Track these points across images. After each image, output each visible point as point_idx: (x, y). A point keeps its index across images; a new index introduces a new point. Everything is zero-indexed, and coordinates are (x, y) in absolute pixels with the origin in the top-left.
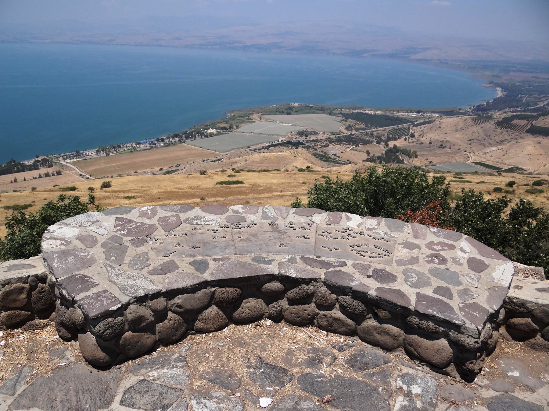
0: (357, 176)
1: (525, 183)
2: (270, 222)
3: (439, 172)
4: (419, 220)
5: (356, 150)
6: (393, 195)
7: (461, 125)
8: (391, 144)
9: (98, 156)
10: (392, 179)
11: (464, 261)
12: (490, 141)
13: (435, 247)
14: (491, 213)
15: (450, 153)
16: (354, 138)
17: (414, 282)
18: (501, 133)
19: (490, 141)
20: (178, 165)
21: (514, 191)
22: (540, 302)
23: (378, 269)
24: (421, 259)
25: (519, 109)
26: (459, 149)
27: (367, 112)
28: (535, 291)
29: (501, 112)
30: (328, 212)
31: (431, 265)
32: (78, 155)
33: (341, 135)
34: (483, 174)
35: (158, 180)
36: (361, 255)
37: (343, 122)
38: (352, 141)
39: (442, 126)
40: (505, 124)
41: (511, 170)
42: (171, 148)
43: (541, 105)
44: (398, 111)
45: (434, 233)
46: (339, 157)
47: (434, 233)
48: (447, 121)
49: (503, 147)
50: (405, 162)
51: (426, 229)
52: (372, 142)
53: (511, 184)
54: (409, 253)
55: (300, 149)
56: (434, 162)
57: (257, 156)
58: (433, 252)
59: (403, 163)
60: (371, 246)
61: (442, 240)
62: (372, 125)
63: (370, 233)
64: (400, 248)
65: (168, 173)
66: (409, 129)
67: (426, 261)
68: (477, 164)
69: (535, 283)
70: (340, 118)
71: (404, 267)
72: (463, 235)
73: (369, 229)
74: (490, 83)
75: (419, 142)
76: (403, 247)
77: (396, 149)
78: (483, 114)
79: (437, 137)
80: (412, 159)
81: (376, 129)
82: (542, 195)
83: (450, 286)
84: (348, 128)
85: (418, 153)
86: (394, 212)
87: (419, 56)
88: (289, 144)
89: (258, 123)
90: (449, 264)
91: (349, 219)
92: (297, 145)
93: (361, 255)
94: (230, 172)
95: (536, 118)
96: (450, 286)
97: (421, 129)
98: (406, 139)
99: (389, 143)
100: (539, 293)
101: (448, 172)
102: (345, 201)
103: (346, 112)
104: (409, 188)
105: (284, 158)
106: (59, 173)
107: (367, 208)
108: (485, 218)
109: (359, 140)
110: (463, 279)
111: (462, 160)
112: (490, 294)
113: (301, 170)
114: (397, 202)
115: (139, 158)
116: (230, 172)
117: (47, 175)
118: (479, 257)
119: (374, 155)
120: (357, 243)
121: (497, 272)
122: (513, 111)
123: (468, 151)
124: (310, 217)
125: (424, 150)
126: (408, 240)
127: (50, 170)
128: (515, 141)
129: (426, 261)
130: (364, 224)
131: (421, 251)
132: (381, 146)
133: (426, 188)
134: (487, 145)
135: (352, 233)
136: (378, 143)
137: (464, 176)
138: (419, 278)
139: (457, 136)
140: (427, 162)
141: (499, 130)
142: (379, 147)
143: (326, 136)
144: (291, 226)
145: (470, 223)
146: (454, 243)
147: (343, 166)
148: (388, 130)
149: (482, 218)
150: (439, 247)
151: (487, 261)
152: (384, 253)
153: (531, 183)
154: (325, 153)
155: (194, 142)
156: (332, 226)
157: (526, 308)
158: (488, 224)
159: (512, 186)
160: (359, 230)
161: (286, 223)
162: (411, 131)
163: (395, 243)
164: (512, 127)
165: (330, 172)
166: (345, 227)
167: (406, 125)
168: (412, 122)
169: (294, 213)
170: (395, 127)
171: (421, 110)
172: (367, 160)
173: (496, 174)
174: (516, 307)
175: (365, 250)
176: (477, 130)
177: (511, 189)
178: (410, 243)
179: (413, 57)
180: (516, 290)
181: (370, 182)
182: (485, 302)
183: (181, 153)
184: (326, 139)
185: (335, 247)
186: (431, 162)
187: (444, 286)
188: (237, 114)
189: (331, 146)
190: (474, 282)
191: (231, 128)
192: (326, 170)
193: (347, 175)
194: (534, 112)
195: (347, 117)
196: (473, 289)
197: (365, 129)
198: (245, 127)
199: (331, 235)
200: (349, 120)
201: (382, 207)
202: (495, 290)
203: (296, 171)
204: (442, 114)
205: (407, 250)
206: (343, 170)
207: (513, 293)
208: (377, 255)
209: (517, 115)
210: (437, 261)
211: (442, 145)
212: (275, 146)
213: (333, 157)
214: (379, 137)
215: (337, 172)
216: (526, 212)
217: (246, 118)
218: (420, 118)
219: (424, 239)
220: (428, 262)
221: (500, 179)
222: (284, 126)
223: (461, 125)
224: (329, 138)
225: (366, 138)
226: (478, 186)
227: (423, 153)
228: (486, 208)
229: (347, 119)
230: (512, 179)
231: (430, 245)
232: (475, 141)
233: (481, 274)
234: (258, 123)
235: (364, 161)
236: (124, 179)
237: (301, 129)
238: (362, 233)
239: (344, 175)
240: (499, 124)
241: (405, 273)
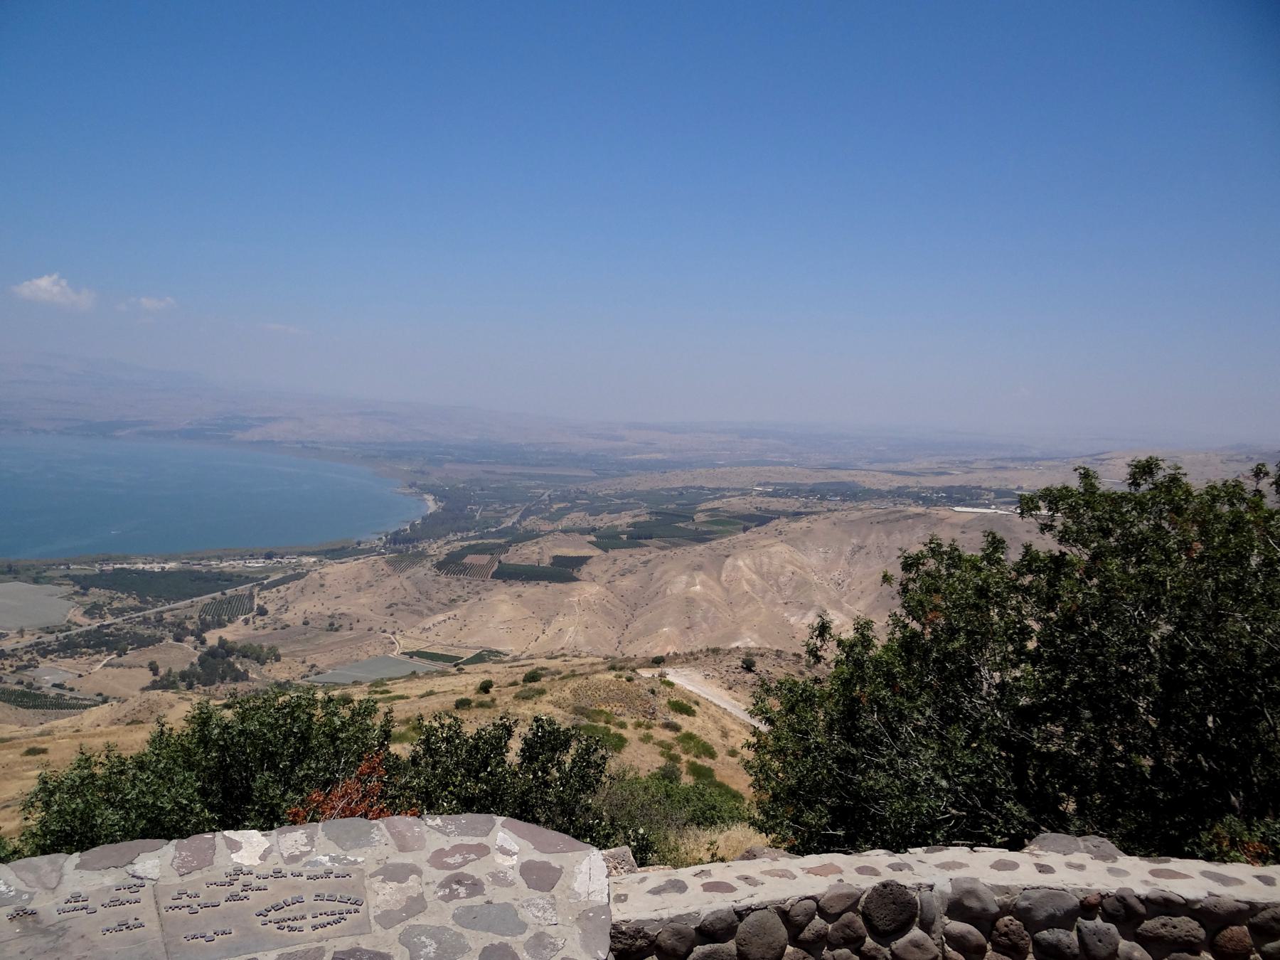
0: (162, 733)
1: (511, 680)
2: (10, 910)
3: (336, 685)
4: (343, 810)
5: (120, 666)
6: (269, 759)
7: (368, 576)
8: (212, 638)
10: (261, 724)
11: (514, 875)
12: (430, 604)
13: (450, 860)
14: (488, 756)
15: (351, 640)
16: (107, 635)
17: (432, 955)
18: (448, 585)
19: (430, 604)
21: (493, 700)
22: (665, 915)
23: (343, 952)
24: (429, 897)
25: (472, 534)
26: (370, 630)
27: (141, 566)
28: (650, 896)
29: (440, 543)
30: (174, 842)
31: (455, 904)
33: (73, 632)
34: (429, 674)
36: (291, 929)
37: (77, 598)
38: (106, 644)
39: (327, 583)
40: (451, 565)
41: (479, 659)
43: (509, 523)
44: (221, 559)
45: (438, 829)
46: (72, 690)
47: (438, 829)
48: (336, 570)
49: (457, 612)
50: (252, 675)
51: (419, 826)
52: (161, 640)
53: (485, 688)
54: (400, 889)
56: (321, 666)
58: (448, 873)
59: (247, 679)
60: (309, 899)
61: (457, 840)
62: (158, 598)
63: (296, 867)
64: (376, 883)
66: (251, 597)
67: (443, 898)
68: (411, 655)
69: (643, 880)
70: (67, 589)
71: (399, 928)
72: (495, 817)
73: (293, 859)
74: (410, 487)
75: (278, 625)
76: (383, 881)
77: (225, 649)
78: (407, 549)
79: (319, 608)
80: (266, 667)
81: (168, 607)
82: (547, 697)
83: (507, 939)
85: (281, 651)
86: (279, 805)
87: (255, 434)
90: (488, 889)
91: (235, 846)
93: (291, 929)
95: (504, 548)
96: (507, 939)
97: (282, 594)
98: (246, 622)
99: (207, 635)
100: (657, 898)
101: (356, 683)
102: (145, 805)
103: (83, 573)
104: (304, 738)
107: (211, 811)
108: (478, 772)
109: (125, 638)
110: (527, 915)
111: (379, 651)
112: (583, 930)
114: (285, 779)
118: (537, 856)
119: (170, 671)
120: (273, 903)
121: (579, 877)
122: (462, 539)
123: (390, 630)
124: (129, 868)
125: (294, 642)
126: (389, 862)
128: (475, 599)
129: (443, 898)
130: (275, 848)
131: (425, 878)
132: (185, 645)
133: (341, 731)
134: (426, 611)
135: (251, 878)
136: (178, 639)
137: (390, 686)
138: (439, 943)
139: (363, 601)
140: (303, 669)
141: (443, 579)
142: (182, 649)
143: (28, 639)
144: (80, 904)
145: (451, 788)
146: (483, 840)
147: (86, 713)
148: (200, 606)
149: (472, 773)
150: (458, 859)
151: (554, 860)
152: (344, 907)
153: (520, 678)
154: (30, 685)
156: (196, 875)
157: (646, 936)
158: (487, 782)
159: (487, 692)
160: (269, 867)
161: (61, 900)
162: (257, 601)
163: (362, 877)
164: (465, 570)
165: (49, 733)
166: (230, 870)
167: (243, 589)
168: (258, 581)
169: (77, 867)
170: (218, 595)
171: (276, 551)
172: (154, 686)
173: (454, 670)
174: (630, 941)
175: (298, 915)
176: (400, 584)
177: (487, 698)
178: (395, 866)
179: (239, 436)
180: (620, 905)
181: (204, 741)
182: (580, 950)
184: (29, 649)
185: (220, 929)
186: (313, 666)
187: (496, 942)
189: (45, 664)
190: (548, 915)
192: (38, 729)
193: (100, 735)
194: (500, 537)
196: (551, 931)
197: (140, 610)
199: (201, 900)
200: (93, 590)
201: (247, 797)
202: (588, 919)
204: (322, 557)
205: (394, 885)
206: (87, 722)
207: (620, 914)
208: (331, 918)
209: (470, 546)
210: (462, 891)
211: (332, 624)
213: (53, 692)
214: (180, 625)
215: (69, 732)
216: (549, 741)
218: (274, 570)
219: (421, 848)
220: (446, 899)
221: (463, 679)
223: (368, 576)
224: (37, 644)
225: (145, 631)
226: (424, 703)
227: (292, 648)
228: (476, 747)
229: (86, 588)
230: (486, 677)
231: (438, 859)
232: (401, 606)
233: (554, 892)
235: (144, 689)
238: (278, 874)
239: (93, 736)
240: (440, 566)
241: (405, 940)
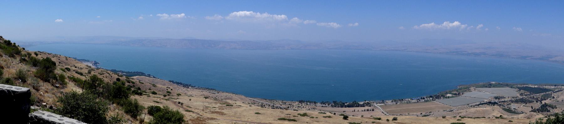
8: (543, 102)
9: (392, 104)
20: (430, 112)
32: (383, 102)
35: (420, 119)
42: (427, 103)
55: (496, 106)
57: (473, 110)
65: (425, 116)
70: (517, 90)
77: (546, 105)
84: (521, 94)
87: (554, 59)
88: (490, 103)
89: (473, 92)
92: (494, 104)
94: (458, 118)
105: (487, 111)
106: (373, 110)
113: (497, 118)
115: (411, 107)
116: (458, 118)
117: (368, 110)
127: (369, 108)
143: (510, 99)
155: (440, 100)
167: (550, 92)
172: (532, 111)
179: (550, 59)
183: (433, 106)
188: (463, 87)
189: (512, 104)
191: (459, 94)
195: (520, 89)
198: (467, 94)
203: (494, 118)
212: (482, 104)
217: (468, 89)
222: (488, 94)
225: (530, 99)
234: (473, 92)
236: (404, 117)
237: (496, 95)
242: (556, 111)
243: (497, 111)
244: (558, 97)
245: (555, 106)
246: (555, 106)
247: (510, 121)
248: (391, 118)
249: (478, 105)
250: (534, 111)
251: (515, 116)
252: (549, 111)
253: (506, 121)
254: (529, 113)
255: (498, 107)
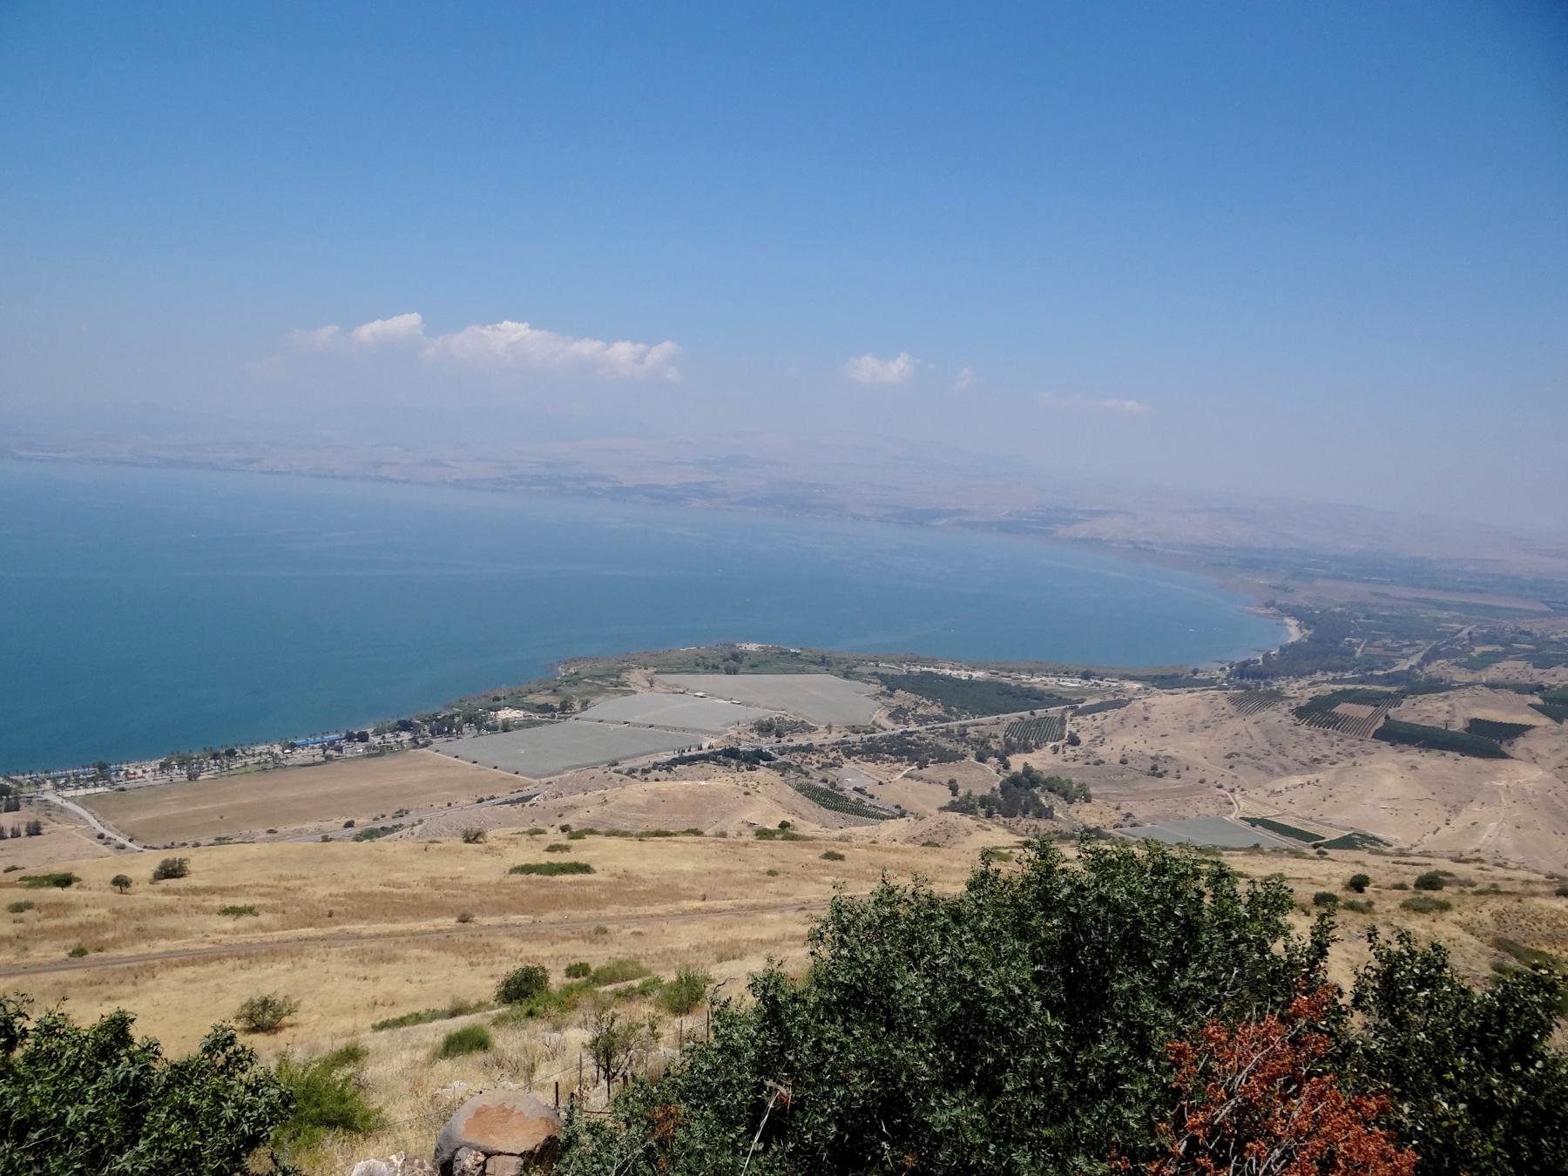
8: (1017, 762)
9: (162, 780)
20: (401, 813)
32: (103, 773)
35: (333, 858)
42: (386, 761)
55: (762, 773)
57: (637, 791)
65: (370, 834)
70: (874, 688)
77: (1029, 779)
84: (898, 714)
88: (730, 756)
89: (644, 695)
92: (754, 759)
94: (554, 836)
106: (34, 830)
113: (763, 834)
115: (284, 789)
116: (554, 836)
143: (835, 737)
155: (457, 745)
167: (1054, 712)
172: (952, 807)
188: (584, 668)
189: (849, 765)
191: (565, 707)
195: (892, 684)
198: (606, 707)
203: (749, 836)
212: (692, 760)
217: (612, 680)
222: (719, 707)
225: (944, 743)
234: (644, 695)
236: (229, 853)
237: (763, 714)
242: (1087, 815)
243: (766, 798)
244: (1100, 739)
245: (1083, 788)
246: (1083, 788)
247: (830, 856)
248: (143, 866)
249: (669, 766)
250: (964, 806)
251: (862, 831)
252: (1046, 813)
253: (812, 856)
254: (934, 819)
255: (775, 776)
